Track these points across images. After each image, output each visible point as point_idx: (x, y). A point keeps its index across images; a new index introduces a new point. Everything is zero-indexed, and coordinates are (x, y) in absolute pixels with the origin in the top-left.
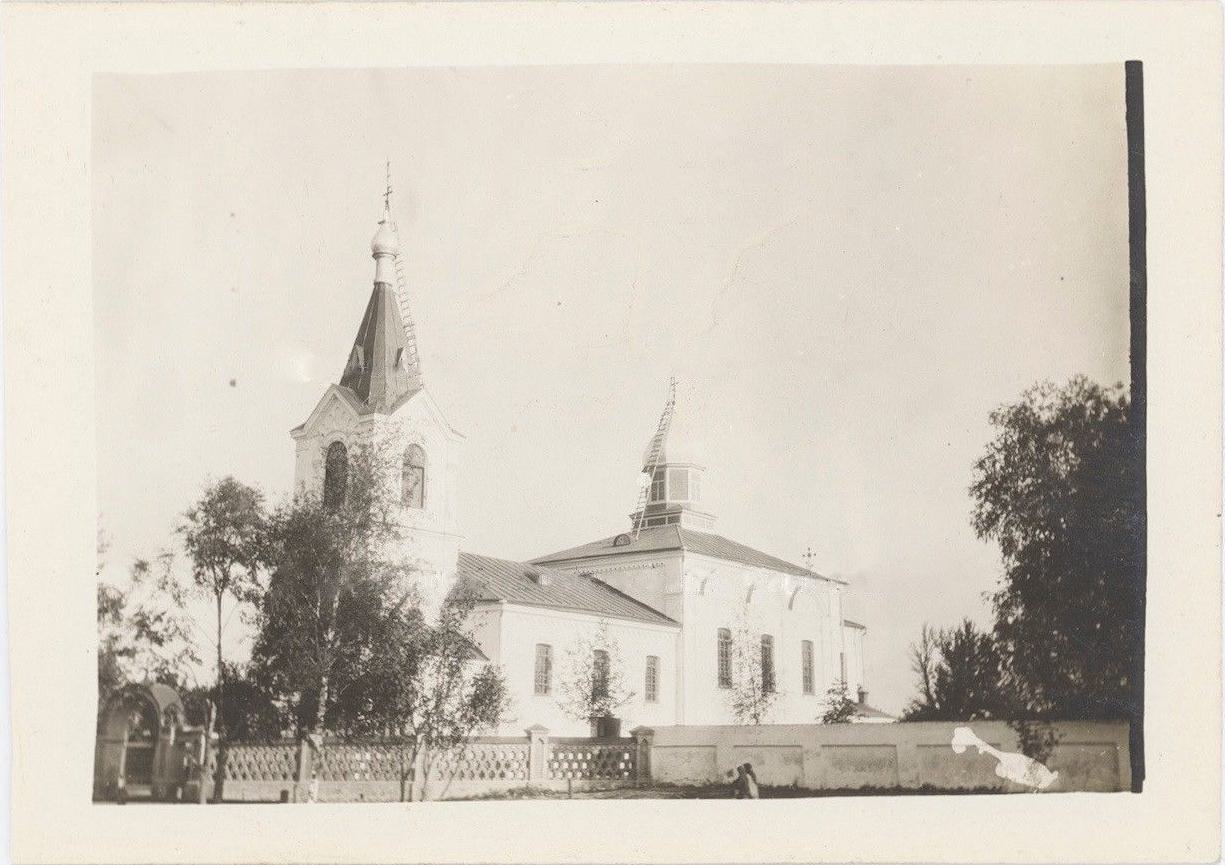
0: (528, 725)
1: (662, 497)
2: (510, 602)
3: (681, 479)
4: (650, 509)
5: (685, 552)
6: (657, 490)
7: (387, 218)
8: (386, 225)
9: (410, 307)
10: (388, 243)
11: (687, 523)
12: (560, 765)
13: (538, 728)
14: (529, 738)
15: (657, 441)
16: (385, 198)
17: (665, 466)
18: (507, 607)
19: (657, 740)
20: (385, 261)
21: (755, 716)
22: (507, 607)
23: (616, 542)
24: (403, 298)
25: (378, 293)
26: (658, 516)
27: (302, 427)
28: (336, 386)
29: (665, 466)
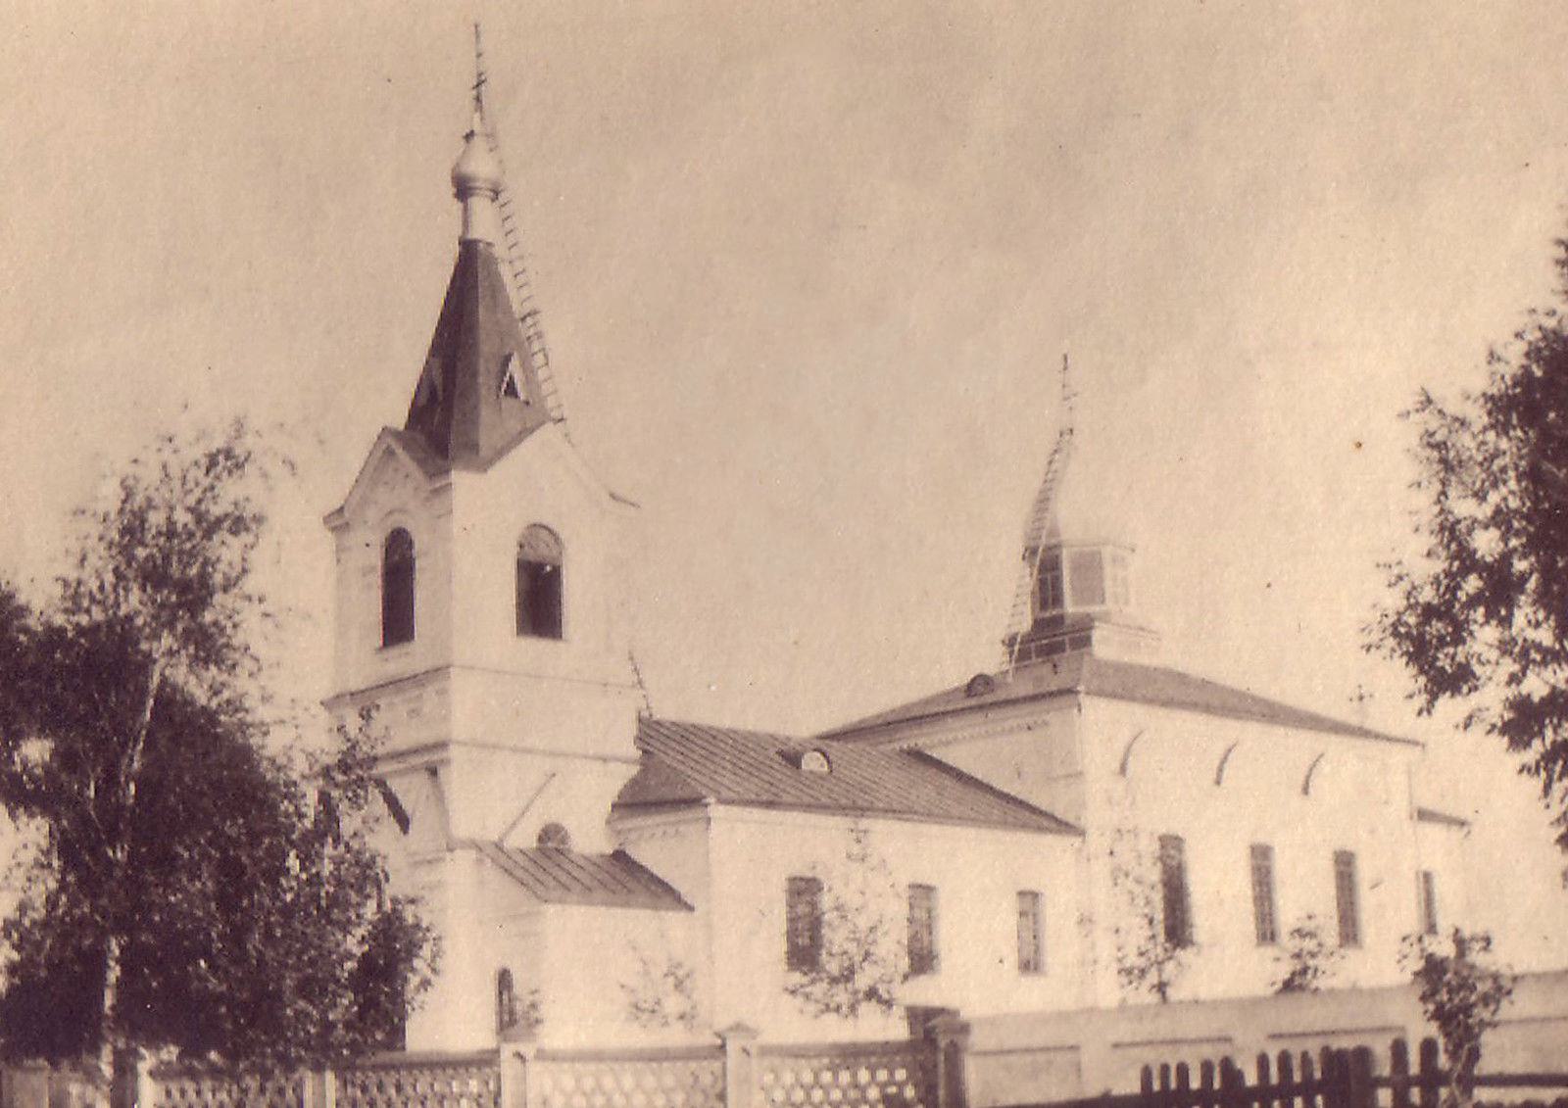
0: (723, 1021)
1: (1057, 600)
2: (722, 801)
3: (1090, 565)
4: (1038, 624)
5: (1082, 697)
6: (1048, 591)
7: (477, 128)
8: (477, 140)
9: (526, 282)
10: (481, 167)
11: (1105, 645)
12: (827, 1093)
13: (738, 1027)
14: (723, 1047)
15: (1043, 502)
16: (474, 92)
17: (1058, 546)
18: (717, 811)
19: (977, 1039)
20: (480, 204)
21: (1161, 987)
22: (717, 811)
23: (971, 689)
24: (518, 266)
25: (470, 271)
26: (1052, 637)
27: (341, 509)
28: (397, 434)
29: (1058, 546)
